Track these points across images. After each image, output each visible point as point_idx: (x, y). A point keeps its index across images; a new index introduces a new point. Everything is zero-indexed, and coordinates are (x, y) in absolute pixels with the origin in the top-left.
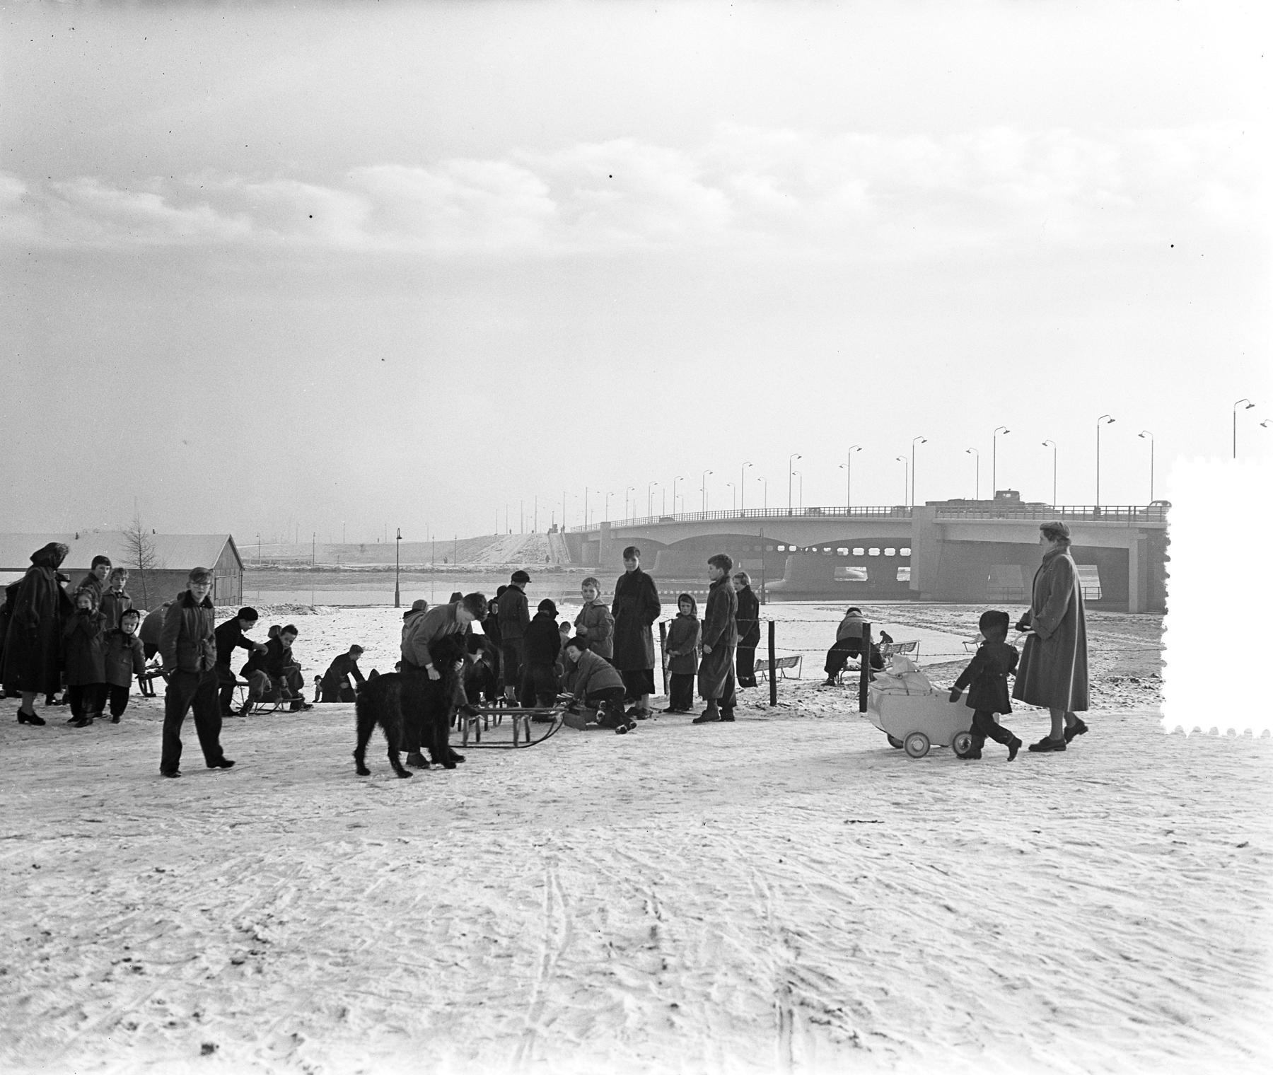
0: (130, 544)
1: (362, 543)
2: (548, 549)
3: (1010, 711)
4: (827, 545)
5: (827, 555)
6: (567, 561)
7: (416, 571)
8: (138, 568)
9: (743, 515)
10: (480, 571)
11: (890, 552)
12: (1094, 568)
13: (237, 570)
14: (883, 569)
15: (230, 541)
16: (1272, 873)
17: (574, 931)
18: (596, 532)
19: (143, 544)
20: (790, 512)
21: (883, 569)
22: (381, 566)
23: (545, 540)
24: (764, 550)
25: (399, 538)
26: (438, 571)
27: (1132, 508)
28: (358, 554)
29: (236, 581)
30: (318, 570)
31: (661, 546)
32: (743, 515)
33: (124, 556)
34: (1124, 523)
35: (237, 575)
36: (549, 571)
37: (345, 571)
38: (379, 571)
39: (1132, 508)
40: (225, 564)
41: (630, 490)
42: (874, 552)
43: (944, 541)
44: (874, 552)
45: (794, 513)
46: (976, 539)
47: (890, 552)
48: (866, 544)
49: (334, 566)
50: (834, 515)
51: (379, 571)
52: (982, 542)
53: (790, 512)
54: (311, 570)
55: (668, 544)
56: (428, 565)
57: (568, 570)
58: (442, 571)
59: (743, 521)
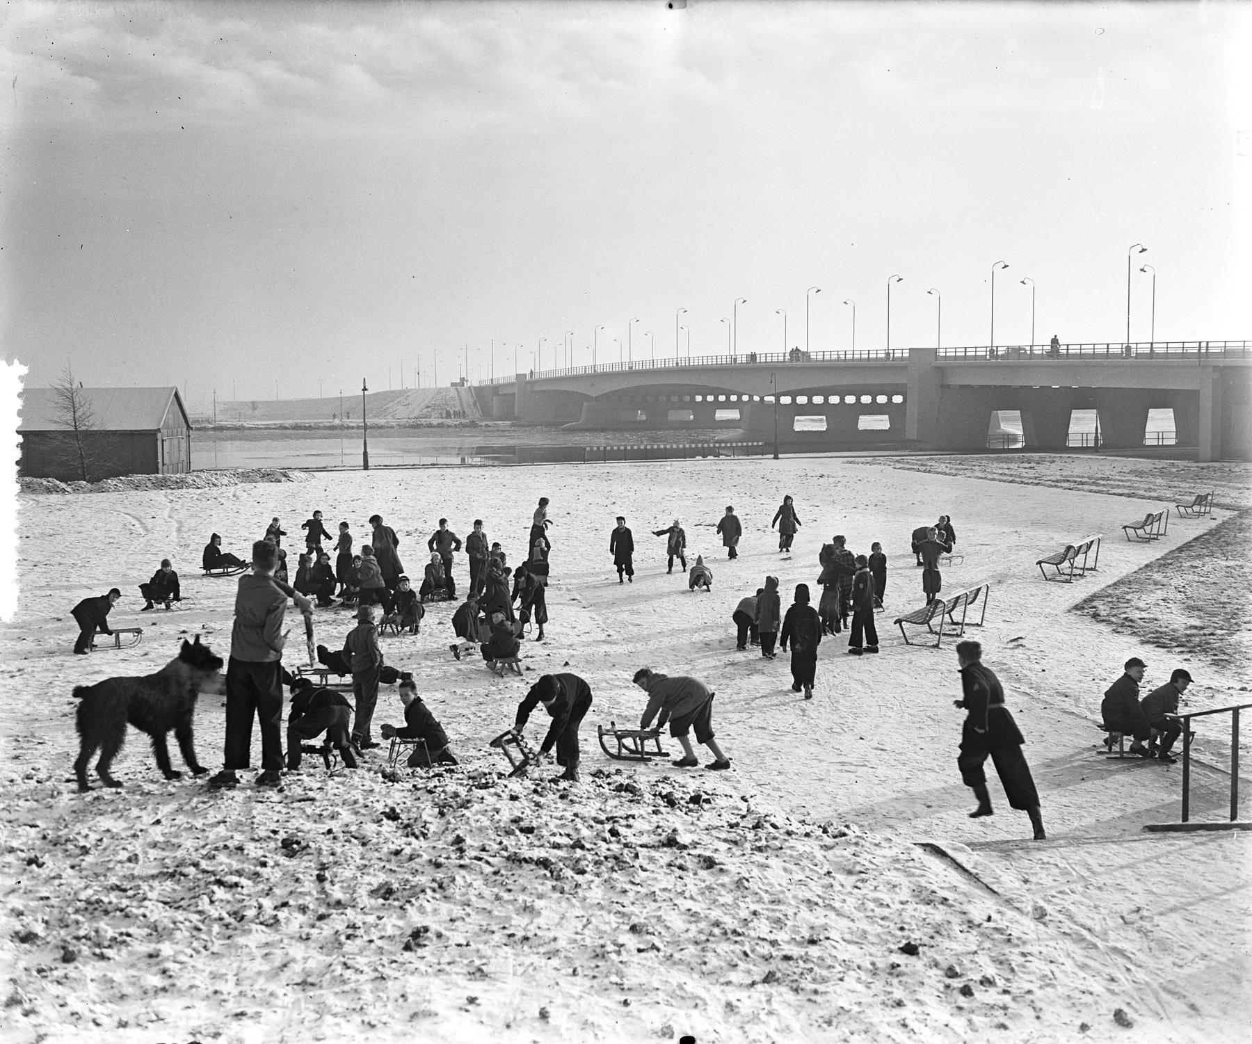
0: (60, 400)
1: (253, 399)
2: (457, 403)
3: (768, 578)
4: (785, 394)
5: (770, 405)
6: (477, 416)
7: (325, 428)
8: (72, 429)
9: (631, 368)
10: (392, 427)
11: (850, 399)
12: (1018, 413)
13: (185, 429)
14: (843, 419)
15: (176, 395)
16: (2, 720)
17: (413, 900)
18: (512, 384)
19: (76, 400)
20: (888, 354)
21: (843, 419)
22: (288, 423)
23: (453, 393)
24: (681, 400)
25: (365, 389)
26: (348, 428)
27: (1204, 345)
28: (250, 412)
29: (184, 445)
30: (221, 428)
31: (587, 398)
32: (631, 368)
33: (57, 415)
34: (1195, 361)
35: (184, 436)
36: (464, 426)
37: (250, 429)
38: (286, 428)
39: (1204, 345)
40: (171, 422)
41: (518, 347)
42: (834, 400)
43: (942, 386)
44: (834, 400)
45: (739, 361)
46: (974, 384)
47: (850, 399)
48: (826, 393)
49: (237, 423)
50: (823, 360)
51: (286, 428)
52: (982, 387)
53: (735, 359)
54: (214, 429)
55: (595, 395)
56: (337, 422)
57: (483, 424)
58: (353, 428)
59: (631, 373)
